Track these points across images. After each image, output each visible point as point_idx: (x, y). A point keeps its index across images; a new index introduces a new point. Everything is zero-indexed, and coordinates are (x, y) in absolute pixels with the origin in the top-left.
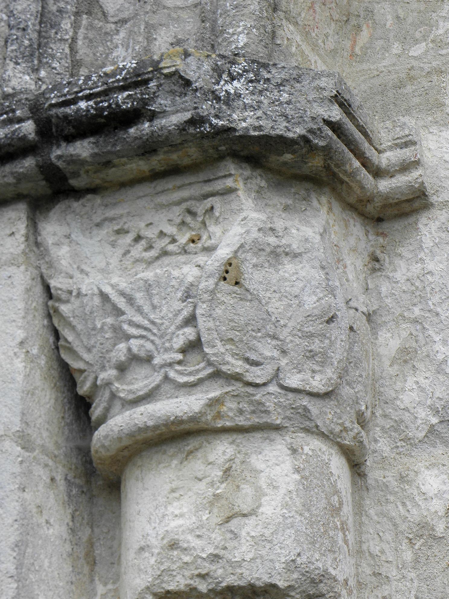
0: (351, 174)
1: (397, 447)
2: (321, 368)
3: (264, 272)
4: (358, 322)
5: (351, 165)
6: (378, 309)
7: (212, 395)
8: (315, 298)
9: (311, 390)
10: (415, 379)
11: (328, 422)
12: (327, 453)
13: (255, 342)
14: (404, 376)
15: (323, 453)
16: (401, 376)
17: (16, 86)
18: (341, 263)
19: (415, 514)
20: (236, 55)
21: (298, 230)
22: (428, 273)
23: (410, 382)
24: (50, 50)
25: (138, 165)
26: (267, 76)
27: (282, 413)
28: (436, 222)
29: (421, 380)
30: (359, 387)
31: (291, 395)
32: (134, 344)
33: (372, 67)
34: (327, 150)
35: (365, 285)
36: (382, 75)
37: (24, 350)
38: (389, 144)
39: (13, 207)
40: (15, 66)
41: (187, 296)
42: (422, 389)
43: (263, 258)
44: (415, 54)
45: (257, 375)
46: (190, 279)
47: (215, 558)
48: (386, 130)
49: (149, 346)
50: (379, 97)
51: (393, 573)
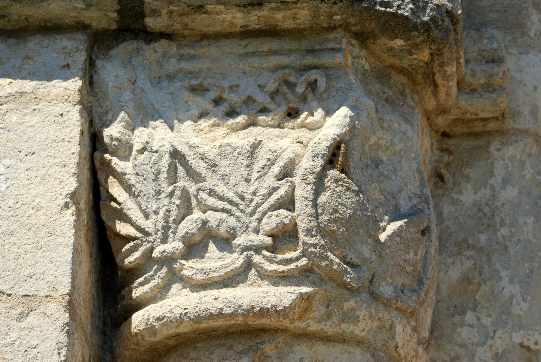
25: (234, 17)
32: (213, 218)
39: (70, 35)
41: (286, 173)
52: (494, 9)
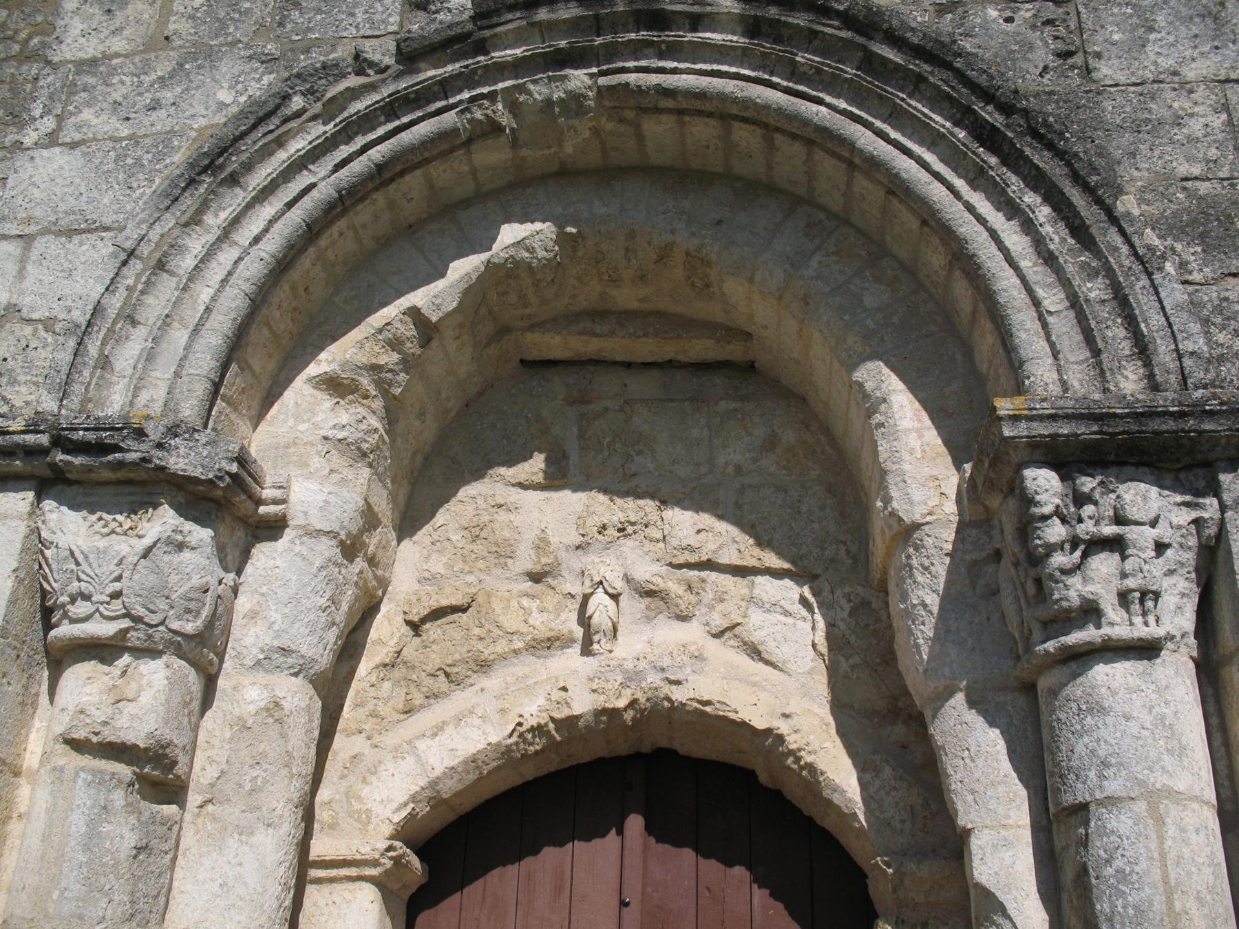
19: (237, 712)
41: (120, 563)
42: (257, 637)
46: (124, 553)
47: (105, 723)
49: (91, 588)
51: (218, 744)
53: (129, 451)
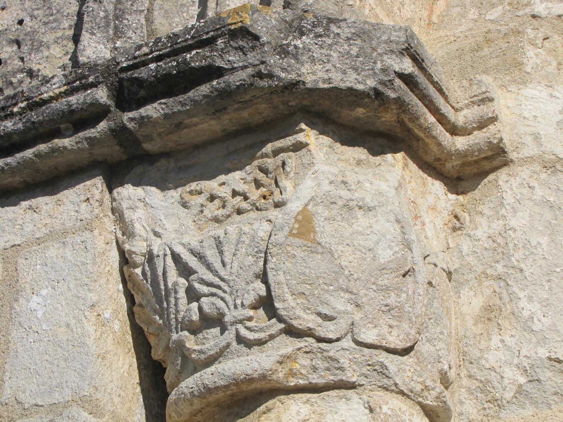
0: (426, 129)
1: (484, 409)
2: (398, 323)
3: (336, 226)
4: (437, 278)
5: (426, 120)
6: (460, 268)
7: (283, 351)
8: (391, 253)
9: (387, 345)
10: (500, 337)
11: (407, 380)
12: (407, 413)
13: (327, 295)
14: (489, 335)
15: (404, 413)
16: (485, 335)
17: (90, 56)
18: (419, 219)
20: (305, 12)
21: (371, 184)
22: (510, 229)
23: (495, 340)
24: (126, 21)
26: (337, 31)
27: (358, 369)
28: (517, 178)
29: (507, 338)
30: (441, 345)
31: (366, 351)
33: (449, 34)
34: (400, 103)
35: (445, 244)
36: (458, 40)
37: (95, 314)
38: (466, 102)
40: (90, 36)
43: (335, 211)
44: (492, 18)
45: (328, 330)
48: (463, 89)
49: (221, 304)
50: (457, 61)
52: (494, 56)
53: (233, 70)
